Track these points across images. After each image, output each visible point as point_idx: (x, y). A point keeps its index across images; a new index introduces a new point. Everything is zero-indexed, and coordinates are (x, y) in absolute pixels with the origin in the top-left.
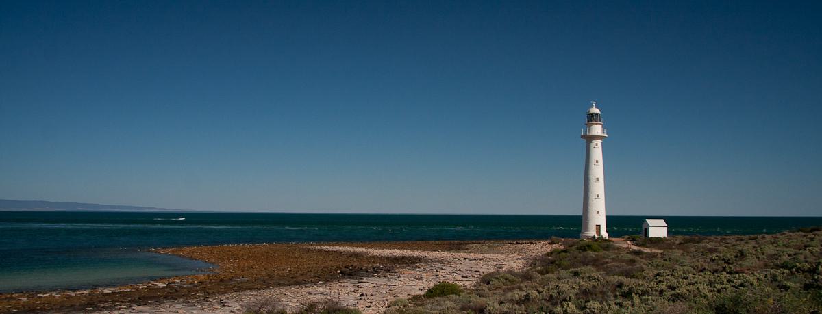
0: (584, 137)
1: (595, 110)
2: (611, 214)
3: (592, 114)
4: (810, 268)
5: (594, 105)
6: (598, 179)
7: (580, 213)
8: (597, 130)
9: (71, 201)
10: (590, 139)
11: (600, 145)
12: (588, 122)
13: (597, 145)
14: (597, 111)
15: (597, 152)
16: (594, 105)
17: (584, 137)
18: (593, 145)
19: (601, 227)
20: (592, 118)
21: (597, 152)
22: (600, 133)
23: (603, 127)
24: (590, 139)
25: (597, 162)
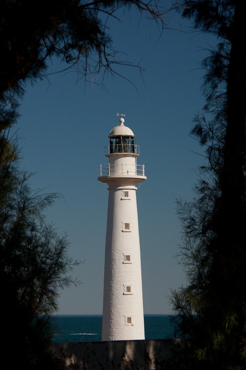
0: (104, 179)
1: (125, 130)
2: (147, 313)
3: (119, 137)
4: (37, 240)
5: (123, 120)
6: (128, 258)
7: (97, 310)
8: (127, 166)
9: (104, 274)
10: (115, 184)
11: (133, 194)
12: (111, 151)
13: (127, 194)
14: (128, 132)
15: (128, 207)
16: (123, 120)
17: (104, 179)
18: (120, 194)
19: (127, 197)
20: (119, 145)
21: (128, 207)
22: (133, 174)
23: (139, 162)
24: (115, 184)
25: (127, 226)
